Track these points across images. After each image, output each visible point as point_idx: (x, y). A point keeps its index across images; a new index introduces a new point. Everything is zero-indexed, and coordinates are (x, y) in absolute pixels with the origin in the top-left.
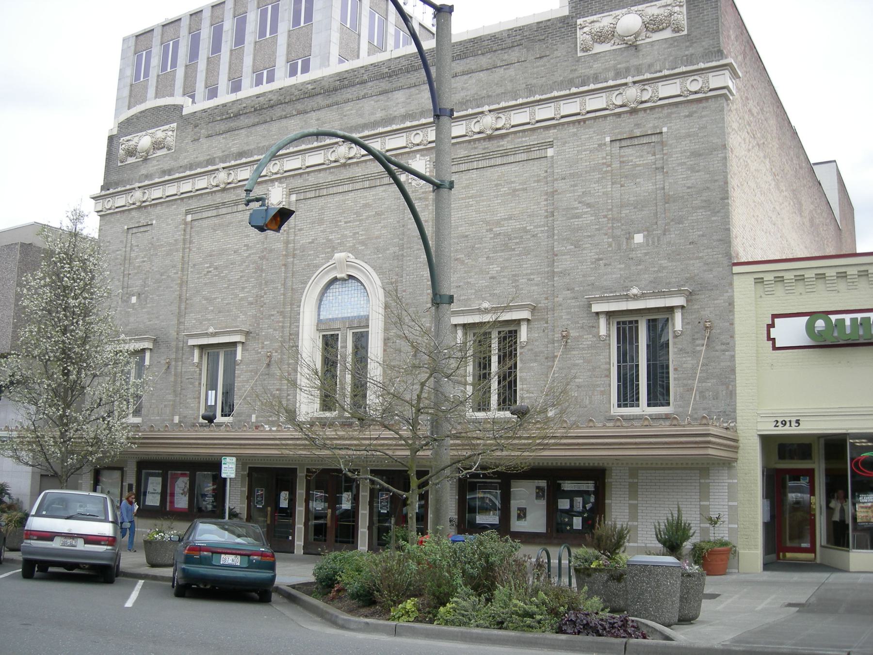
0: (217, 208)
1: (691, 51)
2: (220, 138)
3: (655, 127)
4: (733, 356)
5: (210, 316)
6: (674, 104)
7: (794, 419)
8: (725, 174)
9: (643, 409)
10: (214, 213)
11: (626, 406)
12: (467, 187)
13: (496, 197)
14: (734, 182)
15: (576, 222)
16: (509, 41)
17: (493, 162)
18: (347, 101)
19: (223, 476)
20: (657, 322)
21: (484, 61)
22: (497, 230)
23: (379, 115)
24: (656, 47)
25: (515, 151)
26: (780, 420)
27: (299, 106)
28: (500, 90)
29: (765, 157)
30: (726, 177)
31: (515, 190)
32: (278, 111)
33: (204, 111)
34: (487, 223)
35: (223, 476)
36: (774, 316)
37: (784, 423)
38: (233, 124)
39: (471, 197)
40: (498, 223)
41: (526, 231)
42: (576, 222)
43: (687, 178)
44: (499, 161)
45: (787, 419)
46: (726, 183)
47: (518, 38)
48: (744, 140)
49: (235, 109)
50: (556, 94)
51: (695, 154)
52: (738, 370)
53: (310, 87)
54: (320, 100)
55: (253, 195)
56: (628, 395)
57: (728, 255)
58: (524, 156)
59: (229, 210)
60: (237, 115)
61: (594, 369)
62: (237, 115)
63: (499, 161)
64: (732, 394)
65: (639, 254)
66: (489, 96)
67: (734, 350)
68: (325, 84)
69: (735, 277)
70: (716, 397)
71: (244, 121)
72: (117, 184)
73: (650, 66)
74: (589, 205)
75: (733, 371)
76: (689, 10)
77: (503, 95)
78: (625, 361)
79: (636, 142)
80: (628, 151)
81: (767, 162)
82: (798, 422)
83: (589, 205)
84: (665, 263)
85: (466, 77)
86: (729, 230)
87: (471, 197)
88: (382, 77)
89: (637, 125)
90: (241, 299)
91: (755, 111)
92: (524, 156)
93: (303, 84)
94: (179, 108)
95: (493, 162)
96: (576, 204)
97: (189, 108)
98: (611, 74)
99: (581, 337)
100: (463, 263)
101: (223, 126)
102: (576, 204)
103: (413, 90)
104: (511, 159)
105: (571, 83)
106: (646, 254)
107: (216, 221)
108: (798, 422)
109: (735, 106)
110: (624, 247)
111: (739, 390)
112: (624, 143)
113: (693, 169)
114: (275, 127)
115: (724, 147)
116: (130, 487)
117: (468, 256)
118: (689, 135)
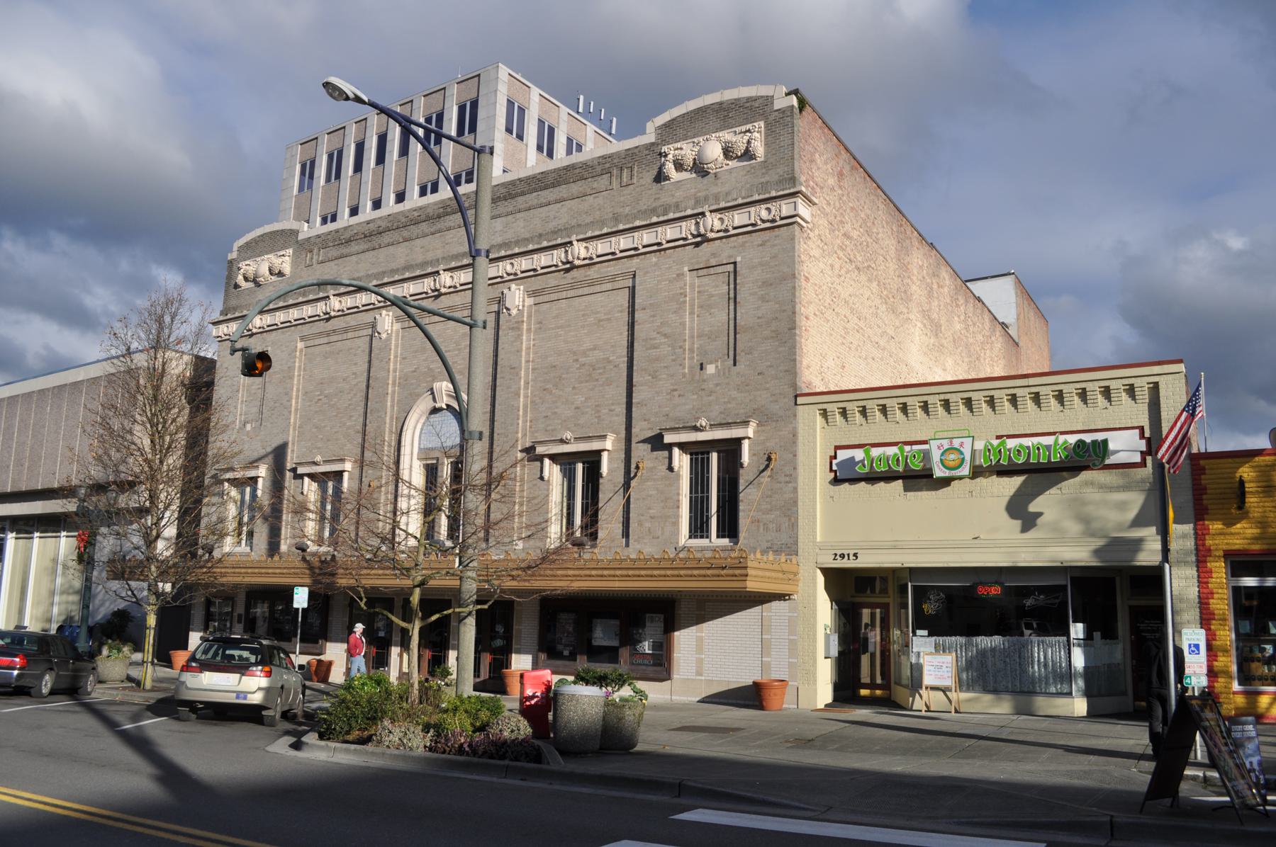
0: (328, 335)
1: (767, 178)
2: (332, 263)
3: (730, 257)
4: (795, 488)
5: (319, 445)
6: (752, 230)
7: (852, 553)
8: (793, 302)
9: (716, 540)
10: (325, 340)
11: (696, 537)
12: (557, 316)
13: (583, 327)
14: (802, 310)
15: (654, 352)
16: (599, 169)
17: (580, 292)
18: (449, 229)
19: (295, 606)
20: (730, 450)
21: (575, 188)
22: (582, 360)
23: (401, 262)
24: (734, 175)
25: (600, 281)
26: (839, 553)
27: (406, 234)
28: (589, 219)
29: (870, 280)
30: (794, 307)
31: (600, 321)
32: (386, 238)
33: (319, 236)
34: (574, 353)
35: (295, 606)
36: (837, 448)
37: (842, 556)
38: (344, 251)
39: (561, 327)
40: (584, 354)
41: (609, 362)
42: (654, 352)
43: (758, 308)
44: (586, 291)
45: (846, 552)
46: (794, 313)
47: (608, 165)
48: (832, 266)
49: (347, 235)
50: (638, 223)
51: (766, 284)
52: (800, 503)
53: (416, 214)
54: (424, 227)
55: (238, 345)
56: (699, 528)
57: (794, 386)
58: (609, 286)
59: (340, 337)
60: (349, 241)
61: (667, 499)
62: (349, 241)
63: (586, 291)
64: (794, 526)
65: (711, 385)
66: (579, 225)
67: (796, 482)
68: (430, 211)
69: (800, 408)
70: (778, 530)
71: (355, 247)
72: (235, 309)
73: (727, 194)
74: (665, 336)
75: (796, 503)
76: (767, 136)
77: (591, 224)
78: (696, 492)
79: (712, 271)
80: (705, 280)
81: (875, 284)
82: (855, 555)
83: (665, 336)
84: (734, 393)
85: (558, 205)
86: (795, 360)
87: (561, 327)
88: (428, 219)
89: (714, 255)
90: (348, 428)
91: (855, 234)
92: (609, 286)
93: (409, 211)
94: (294, 233)
95: (580, 292)
96: (654, 335)
97: (305, 231)
98: (692, 202)
99: (655, 468)
100: (551, 393)
101: (334, 252)
102: (654, 335)
103: (510, 217)
104: (598, 288)
105: (653, 211)
106: (717, 385)
107: (327, 348)
108: (855, 555)
109: (817, 232)
110: (697, 377)
111: (800, 524)
112: (701, 273)
113: (764, 299)
114: (382, 254)
115: (794, 276)
116: (240, 616)
117: (556, 386)
118: (761, 264)
